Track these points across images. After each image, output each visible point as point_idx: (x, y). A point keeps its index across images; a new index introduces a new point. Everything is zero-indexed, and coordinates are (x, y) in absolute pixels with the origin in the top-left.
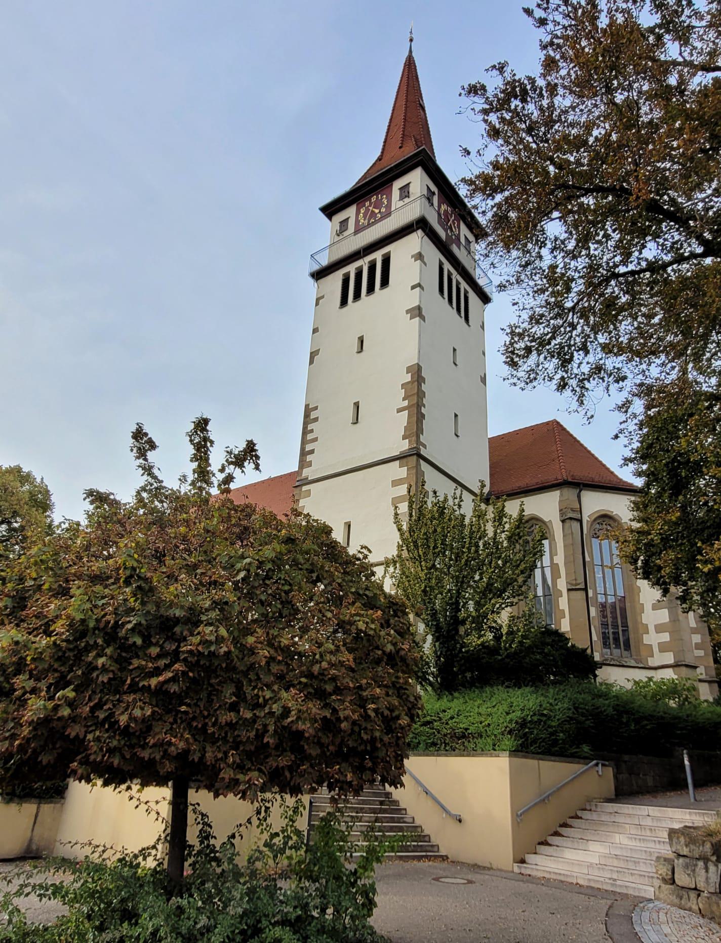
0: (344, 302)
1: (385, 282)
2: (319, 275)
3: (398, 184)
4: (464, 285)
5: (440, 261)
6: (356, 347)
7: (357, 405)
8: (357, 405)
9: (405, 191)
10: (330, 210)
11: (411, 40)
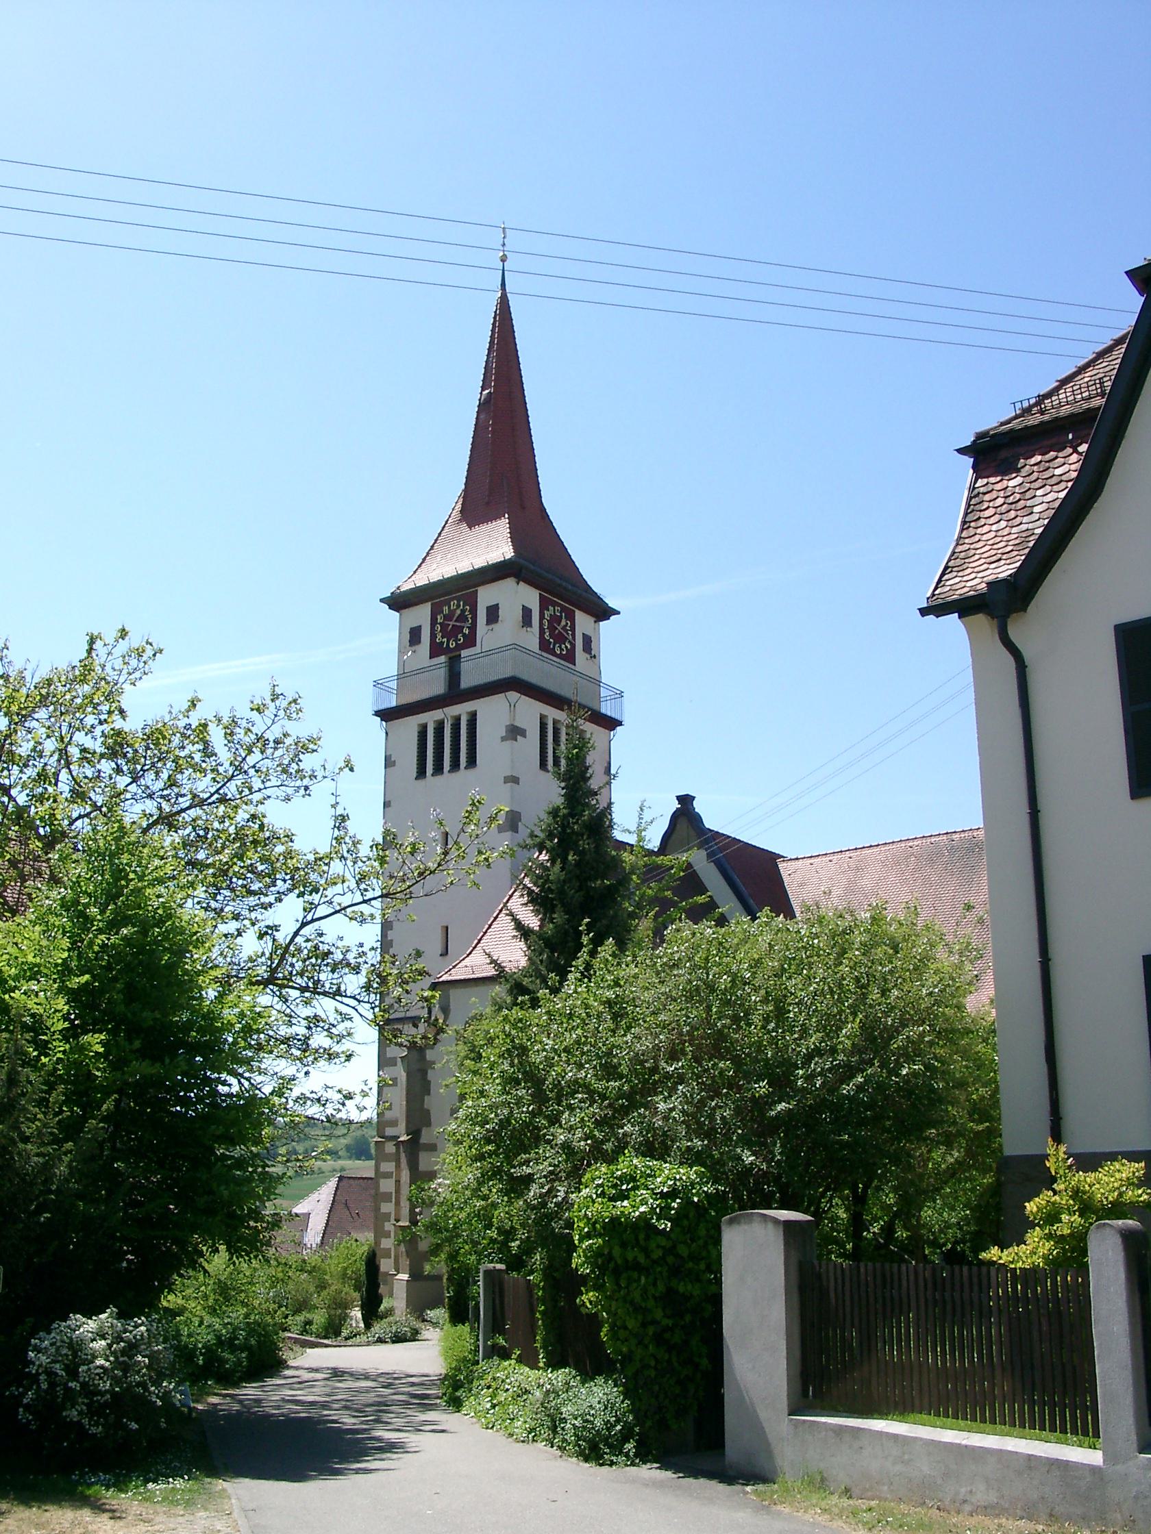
0: (421, 773)
1: (472, 762)
3: (486, 596)
5: (543, 719)
6: (439, 949)
9: (493, 614)
11: (504, 245)
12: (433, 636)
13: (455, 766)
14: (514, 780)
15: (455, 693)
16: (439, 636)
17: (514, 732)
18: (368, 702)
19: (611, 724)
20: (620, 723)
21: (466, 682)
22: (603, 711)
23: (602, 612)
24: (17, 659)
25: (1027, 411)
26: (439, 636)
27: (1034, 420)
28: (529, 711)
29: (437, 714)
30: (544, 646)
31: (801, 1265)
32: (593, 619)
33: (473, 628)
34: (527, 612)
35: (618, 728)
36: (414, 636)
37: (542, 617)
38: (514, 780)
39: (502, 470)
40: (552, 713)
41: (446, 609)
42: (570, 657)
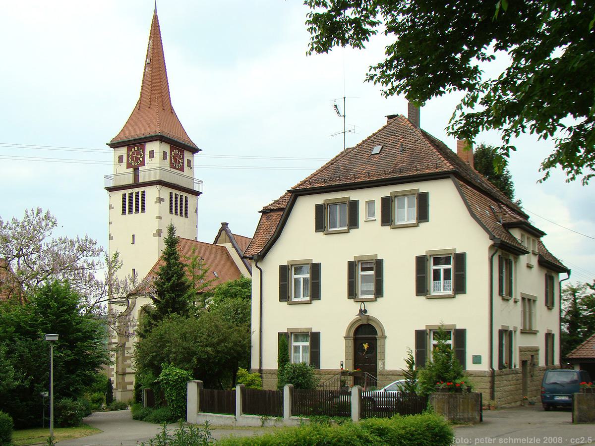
0: (124, 212)
1: (143, 209)
2: (110, 189)
3: (149, 147)
4: (184, 195)
6: (131, 241)
7: (133, 236)
8: (133, 236)
9: (152, 154)
10: (114, 145)
12: (128, 160)
13: (137, 210)
14: (160, 218)
15: (136, 184)
16: (130, 160)
17: (160, 200)
18: (103, 184)
19: (197, 194)
20: (201, 193)
21: (141, 180)
22: (195, 189)
23: (194, 150)
24: (6, 220)
25: (299, 185)
26: (130, 160)
27: (301, 187)
28: (166, 193)
29: (130, 191)
30: (172, 166)
31: (200, 390)
32: (191, 153)
33: (144, 158)
34: (165, 153)
35: (201, 195)
36: (121, 159)
37: (171, 154)
38: (160, 218)
39: (156, 10)
40: (174, 192)
41: (133, 149)
42: (182, 169)
